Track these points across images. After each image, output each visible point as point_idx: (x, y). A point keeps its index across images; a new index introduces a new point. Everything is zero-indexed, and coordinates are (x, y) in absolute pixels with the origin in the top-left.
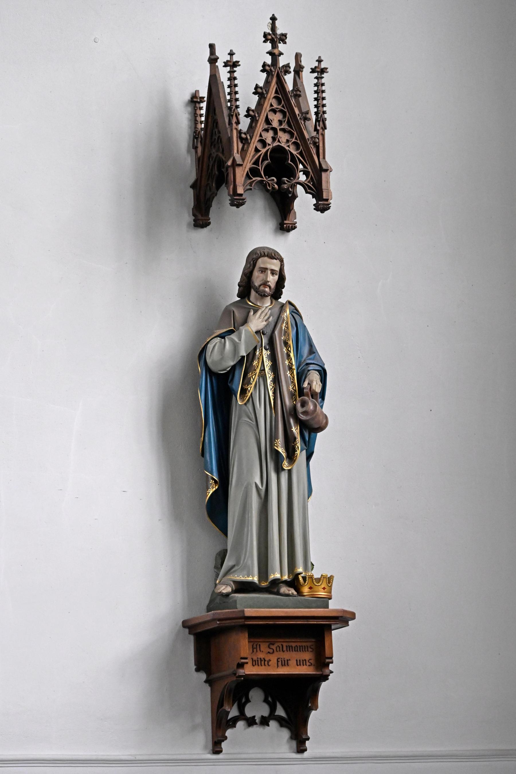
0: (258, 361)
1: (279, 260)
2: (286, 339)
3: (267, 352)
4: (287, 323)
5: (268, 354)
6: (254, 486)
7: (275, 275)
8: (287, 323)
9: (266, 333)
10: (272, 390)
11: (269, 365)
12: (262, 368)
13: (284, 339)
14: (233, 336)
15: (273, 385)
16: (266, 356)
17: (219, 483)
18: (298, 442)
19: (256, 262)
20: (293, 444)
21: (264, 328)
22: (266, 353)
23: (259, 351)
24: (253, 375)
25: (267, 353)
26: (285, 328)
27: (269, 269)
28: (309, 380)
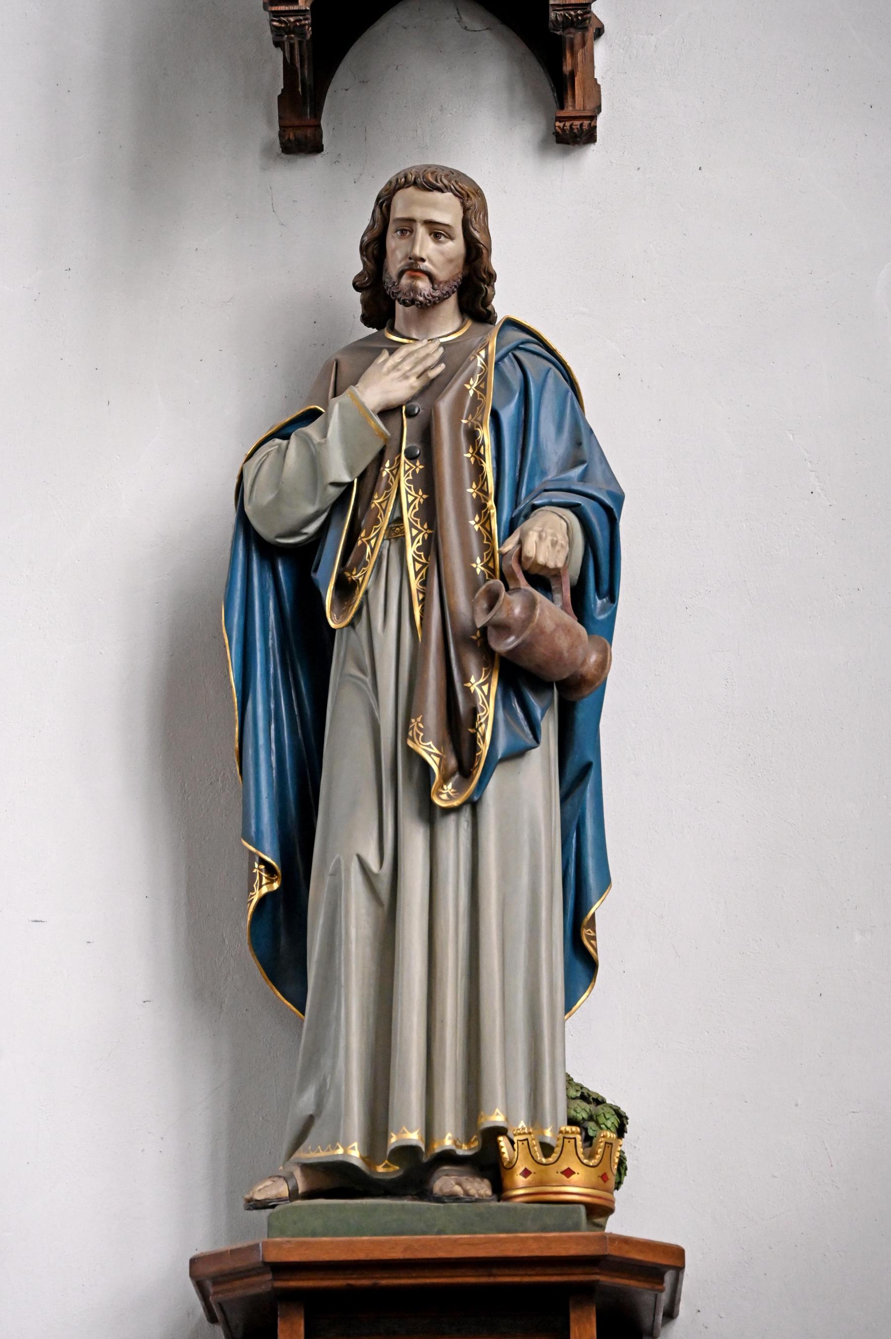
0: (387, 494)
1: (452, 191)
2: (475, 423)
3: (415, 465)
4: (484, 379)
5: (418, 470)
6: (355, 866)
7: (443, 238)
8: (484, 379)
9: (419, 411)
10: (419, 576)
11: (417, 502)
12: (397, 515)
13: (470, 424)
14: (312, 430)
15: (424, 561)
16: (411, 477)
17: (279, 871)
18: (483, 720)
19: (389, 207)
20: (470, 730)
21: (414, 398)
22: (409, 470)
23: (391, 465)
24: (372, 538)
25: (415, 467)
26: (478, 392)
27: (418, 220)
28: (522, 530)
